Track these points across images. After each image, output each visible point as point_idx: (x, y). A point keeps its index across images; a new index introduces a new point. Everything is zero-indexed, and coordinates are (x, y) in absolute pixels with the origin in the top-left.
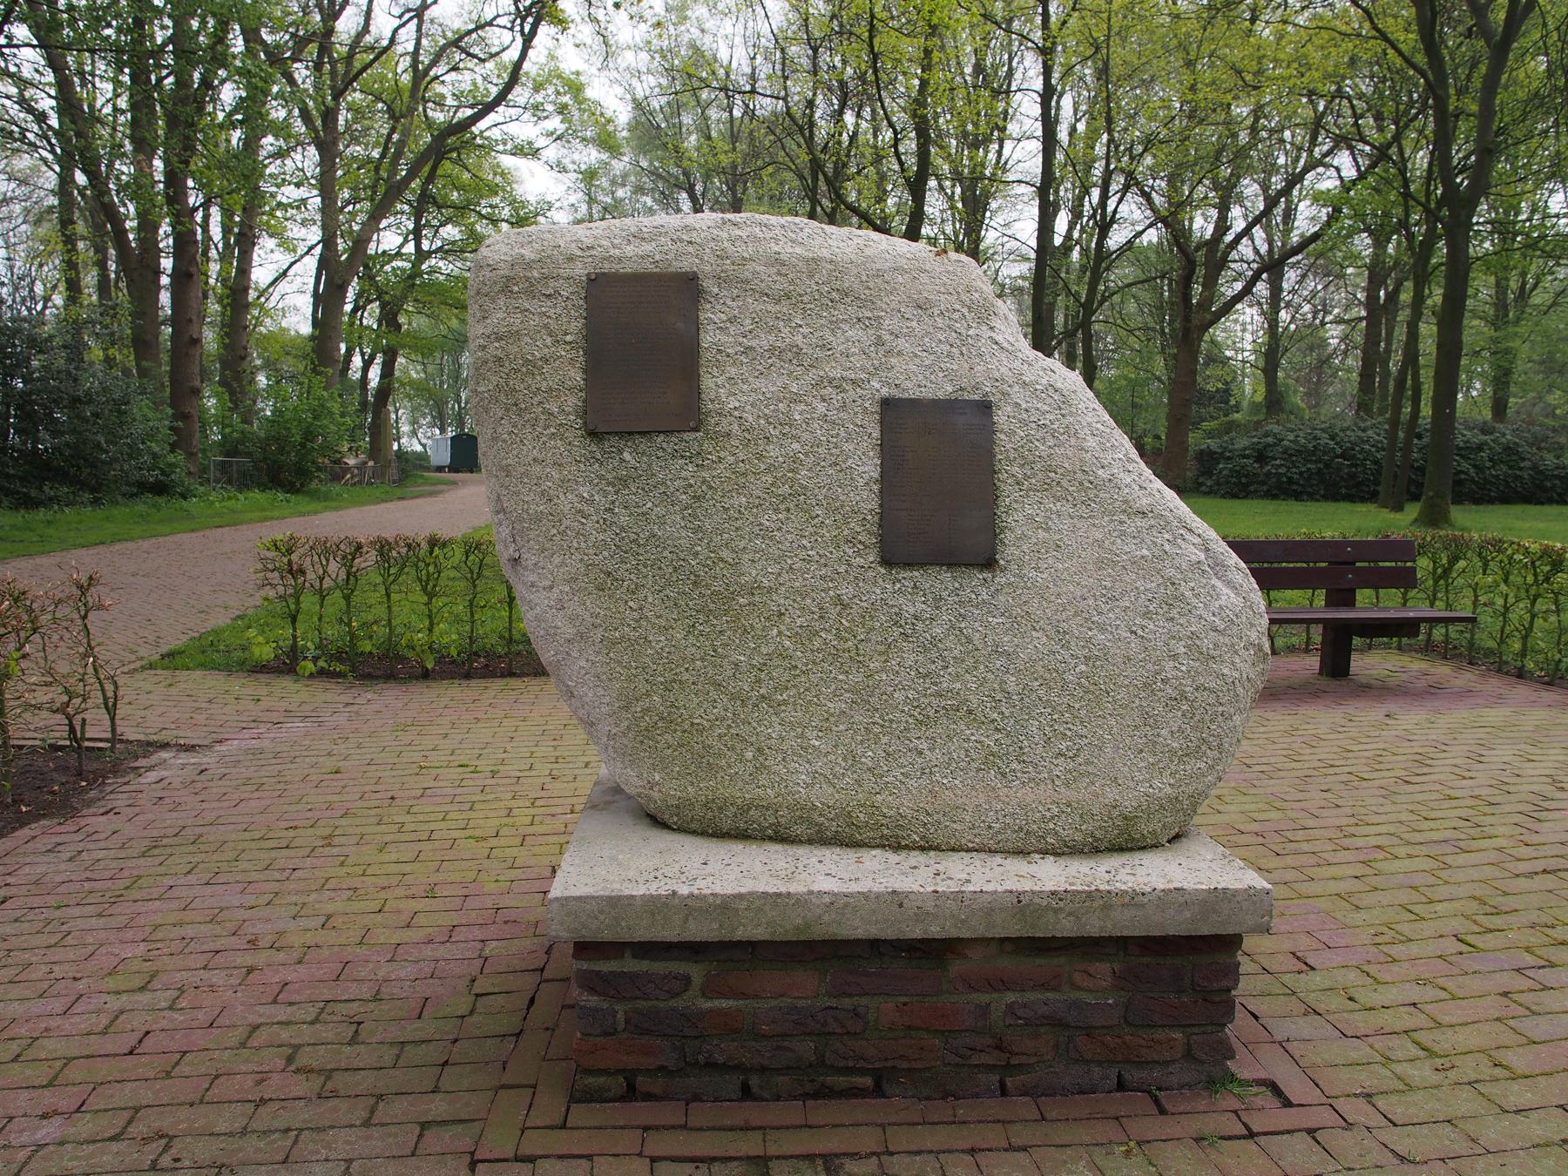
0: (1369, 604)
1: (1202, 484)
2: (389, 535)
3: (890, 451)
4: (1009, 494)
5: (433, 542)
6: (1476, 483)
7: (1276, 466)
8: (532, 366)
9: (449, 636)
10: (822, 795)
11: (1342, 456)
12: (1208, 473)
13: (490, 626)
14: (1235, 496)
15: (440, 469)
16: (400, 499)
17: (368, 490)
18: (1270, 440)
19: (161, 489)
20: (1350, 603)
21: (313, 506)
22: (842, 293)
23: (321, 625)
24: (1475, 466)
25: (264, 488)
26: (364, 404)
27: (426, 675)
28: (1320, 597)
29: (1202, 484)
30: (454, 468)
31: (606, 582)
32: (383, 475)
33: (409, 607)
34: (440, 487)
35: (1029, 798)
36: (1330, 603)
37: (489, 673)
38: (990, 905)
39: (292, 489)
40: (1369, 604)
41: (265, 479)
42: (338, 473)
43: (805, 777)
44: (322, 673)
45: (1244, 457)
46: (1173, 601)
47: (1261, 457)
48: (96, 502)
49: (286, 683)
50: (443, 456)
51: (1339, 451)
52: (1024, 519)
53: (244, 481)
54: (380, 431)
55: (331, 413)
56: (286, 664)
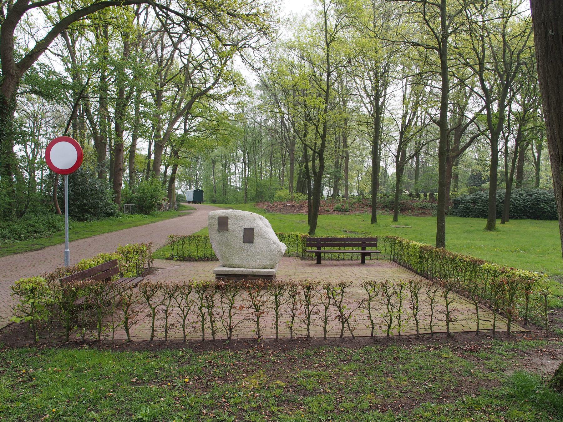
0: (368, 249)
1: (454, 212)
2: (190, 235)
3: (244, 233)
4: (255, 237)
5: (198, 236)
6: (550, 212)
7: (478, 206)
8: (214, 225)
9: (201, 254)
10: (238, 263)
11: (502, 203)
12: (456, 208)
13: (208, 252)
14: (465, 216)
15: (189, 202)
16: (180, 216)
17: (169, 213)
18: (478, 197)
19: (110, 215)
20: (365, 250)
21: (154, 219)
22: (241, 218)
23: (178, 250)
24: (550, 207)
25: (138, 213)
26: (165, 182)
27: (196, 261)
28: (360, 248)
29: (454, 212)
30: (195, 202)
31: (219, 244)
32: (172, 207)
33: (193, 248)
34: (191, 211)
35: (256, 264)
36: (362, 250)
37: (208, 260)
38: (250, 272)
39: (147, 213)
40: (368, 249)
41: (139, 210)
42: (160, 207)
43: (236, 262)
44: (178, 260)
45: (469, 203)
46: (269, 246)
47: (474, 202)
48: (97, 219)
49: (172, 261)
50: (190, 196)
51: (501, 201)
52: (256, 239)
53: (133, 211)
54: (171, 189)
55: (159, 190)
56: (171, 258)
